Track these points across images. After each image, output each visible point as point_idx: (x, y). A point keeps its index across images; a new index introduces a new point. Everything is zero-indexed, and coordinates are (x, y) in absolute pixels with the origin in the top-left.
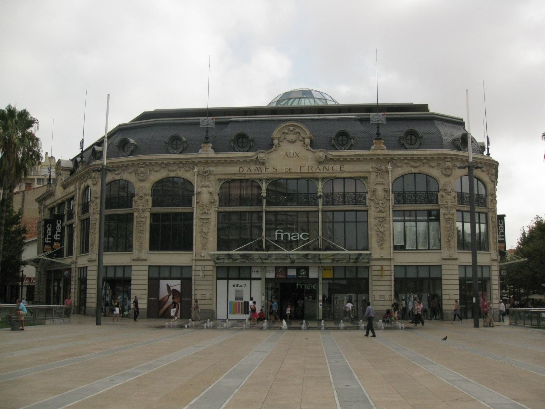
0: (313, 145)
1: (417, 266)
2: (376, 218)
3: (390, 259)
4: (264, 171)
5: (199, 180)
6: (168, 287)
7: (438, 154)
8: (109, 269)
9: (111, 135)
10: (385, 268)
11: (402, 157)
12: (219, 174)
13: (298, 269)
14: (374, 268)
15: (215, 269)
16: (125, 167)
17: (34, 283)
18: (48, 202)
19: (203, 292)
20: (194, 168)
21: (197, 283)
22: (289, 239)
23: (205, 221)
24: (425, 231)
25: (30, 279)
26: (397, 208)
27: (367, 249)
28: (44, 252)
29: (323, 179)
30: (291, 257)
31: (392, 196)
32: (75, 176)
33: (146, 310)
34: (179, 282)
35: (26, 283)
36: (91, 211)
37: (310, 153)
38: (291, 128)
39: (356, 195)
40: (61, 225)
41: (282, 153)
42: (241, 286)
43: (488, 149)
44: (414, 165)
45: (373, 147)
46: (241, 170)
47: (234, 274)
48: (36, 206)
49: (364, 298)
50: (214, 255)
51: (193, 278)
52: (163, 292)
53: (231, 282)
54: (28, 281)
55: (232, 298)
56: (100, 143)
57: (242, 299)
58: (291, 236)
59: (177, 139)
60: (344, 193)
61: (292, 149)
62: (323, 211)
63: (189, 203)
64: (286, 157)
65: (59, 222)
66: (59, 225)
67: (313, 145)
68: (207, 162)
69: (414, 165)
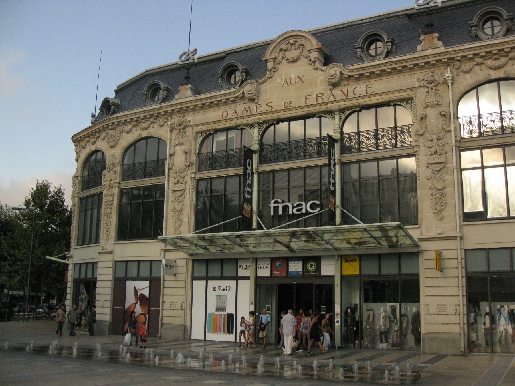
1: (488, 250)
4: (254, 112)
6: (136, 291)
10: (445, 254)
12: (198, 125)
15: (190, 263)
19: (173, 299)
22: (290, 212)
33: (108, 323)
34: (147, 283)
39: (396, 131)
41: (279, 80)
42: (223, 290)
46: (225, 113)
47: (215, 270)
49: (414, 310)
52: (130, 299)
53: (212, 284)
55: (212, 309)
57: (224, 309)
58: (293, 207)
60: (377, 130)
64: (286, 85)
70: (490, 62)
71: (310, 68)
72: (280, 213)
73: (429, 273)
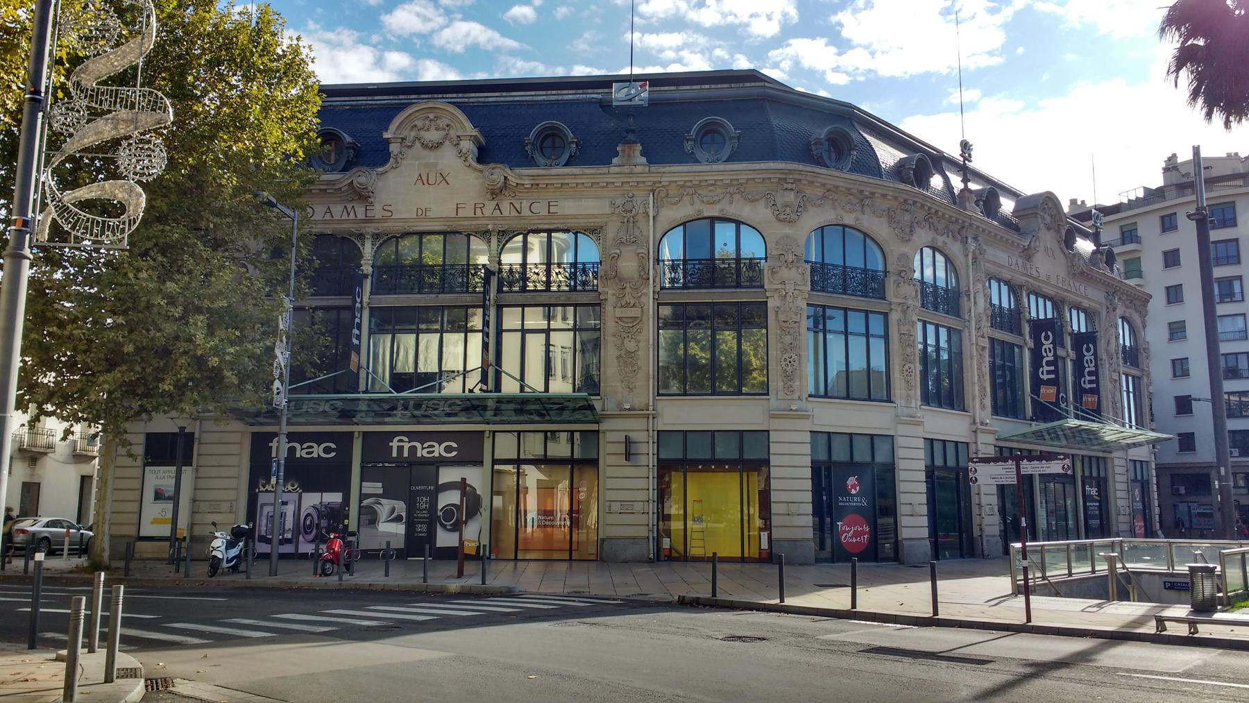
0: (484, 155)
39: (576, 268)
59: (553, 135)
67: (484, 155)
71: (458, 163)
72: (406, 455)
73: (611, 460)
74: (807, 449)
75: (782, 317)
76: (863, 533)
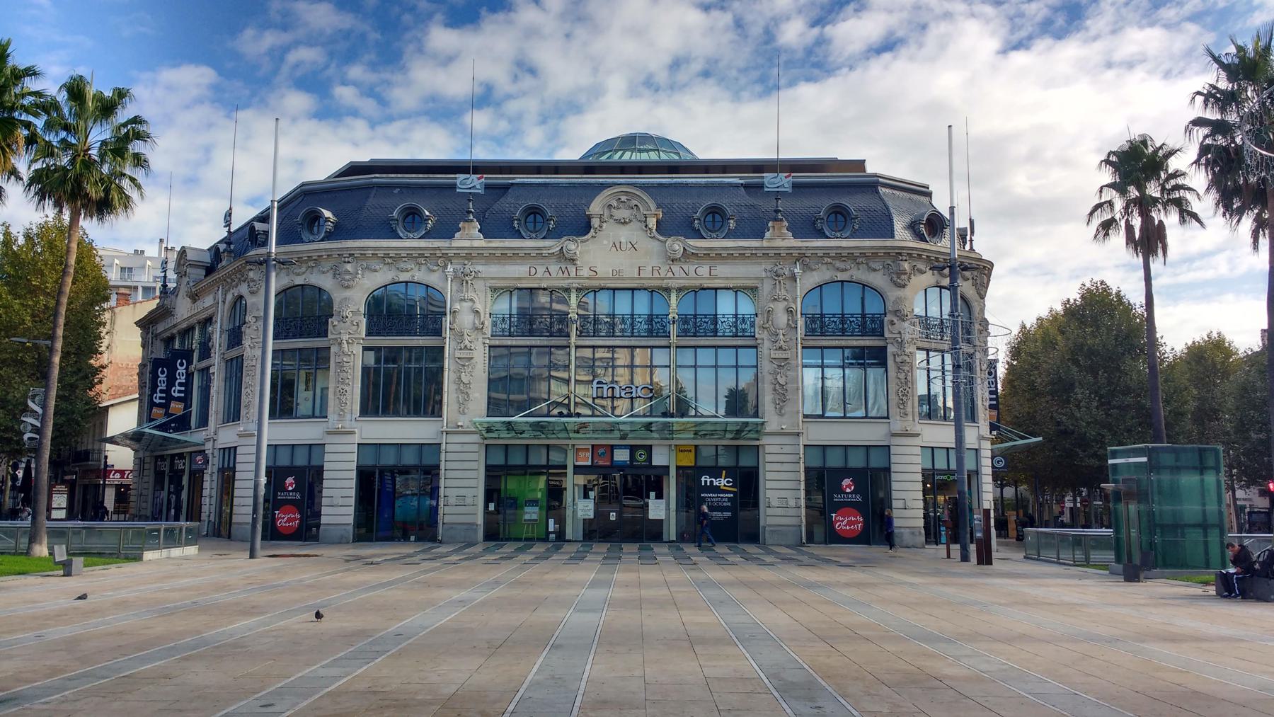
0: (663, 228)
2: (772, 360)
3: (798, 434)
5: (455, 288)
7: (885, 247)
8: (280, 450)
9: (286, 204)
11: (820, 253)
13: (633, 449)
14: (768, 449)
16: (314, 261)
17: (129, 480)
18: (160, 328)
20: (445, 267)
21: (450, 474)
23: (465, 362)
24: (815, 384)
25: (122, 472)
26: (811, 343)
27: (756, 415)
28: (151, 420)
29: (679, 290)
30: (622, 427)
31: (801, 322)
32: (215, 276)
35: (115, 479)
36: (247, 342)
37: (656, 243)
38: (624, 198)
40: (187, 369)
43: (971, 241)
44: (842, 265)
45: (768, 235)
46: (533, 271)
48: (136, 335)
50: (481, 423)
51: (442, 467)
54: (118, 476)
56: (264, 218)
61: (625, 234)
62: (577, 347)
63: (438, 332)
65: (182, 365)
66: (181, 370)
67: (663, 228)
68: (470, 255)
69: (842, 265)
70: (838, 264)
74: (919, 459)
75: (898, 359)
76: (295, 519)
